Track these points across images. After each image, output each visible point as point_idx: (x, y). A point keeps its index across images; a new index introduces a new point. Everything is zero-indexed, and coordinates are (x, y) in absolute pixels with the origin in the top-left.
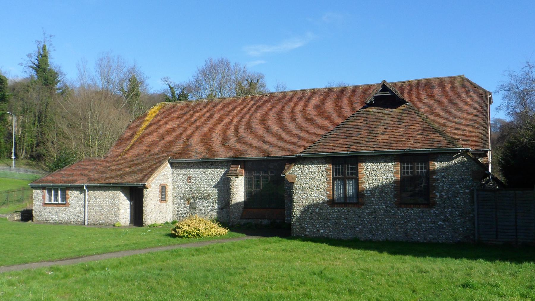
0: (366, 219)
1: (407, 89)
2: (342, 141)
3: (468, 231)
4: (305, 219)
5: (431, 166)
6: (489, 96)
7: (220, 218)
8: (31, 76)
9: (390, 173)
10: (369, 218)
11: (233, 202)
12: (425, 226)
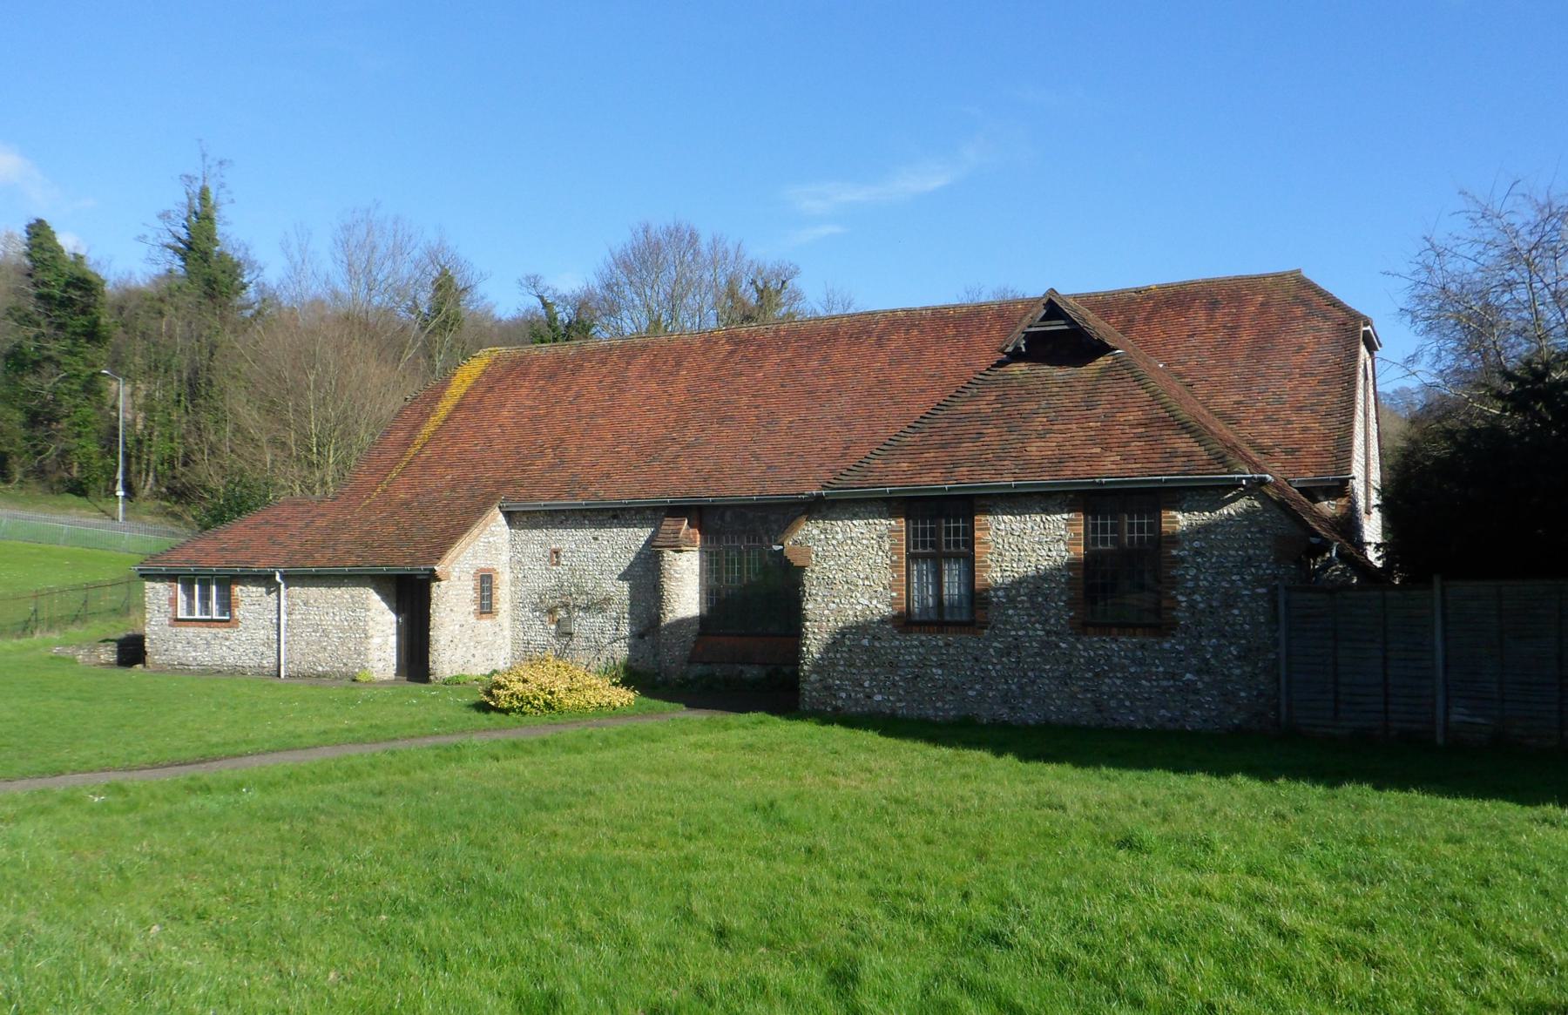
0: (994, 665)
1: (1144, 309)
2: (932, 455)
3: (1262, 700)
4: (834, 664)
5: (1166, 522)
6: (1365, 329)
7: (637, 660)
8: (170, 271)
9: (1058, 541)
10: (1001, 662)
11: (668, 619)
12: (1148, 684)
